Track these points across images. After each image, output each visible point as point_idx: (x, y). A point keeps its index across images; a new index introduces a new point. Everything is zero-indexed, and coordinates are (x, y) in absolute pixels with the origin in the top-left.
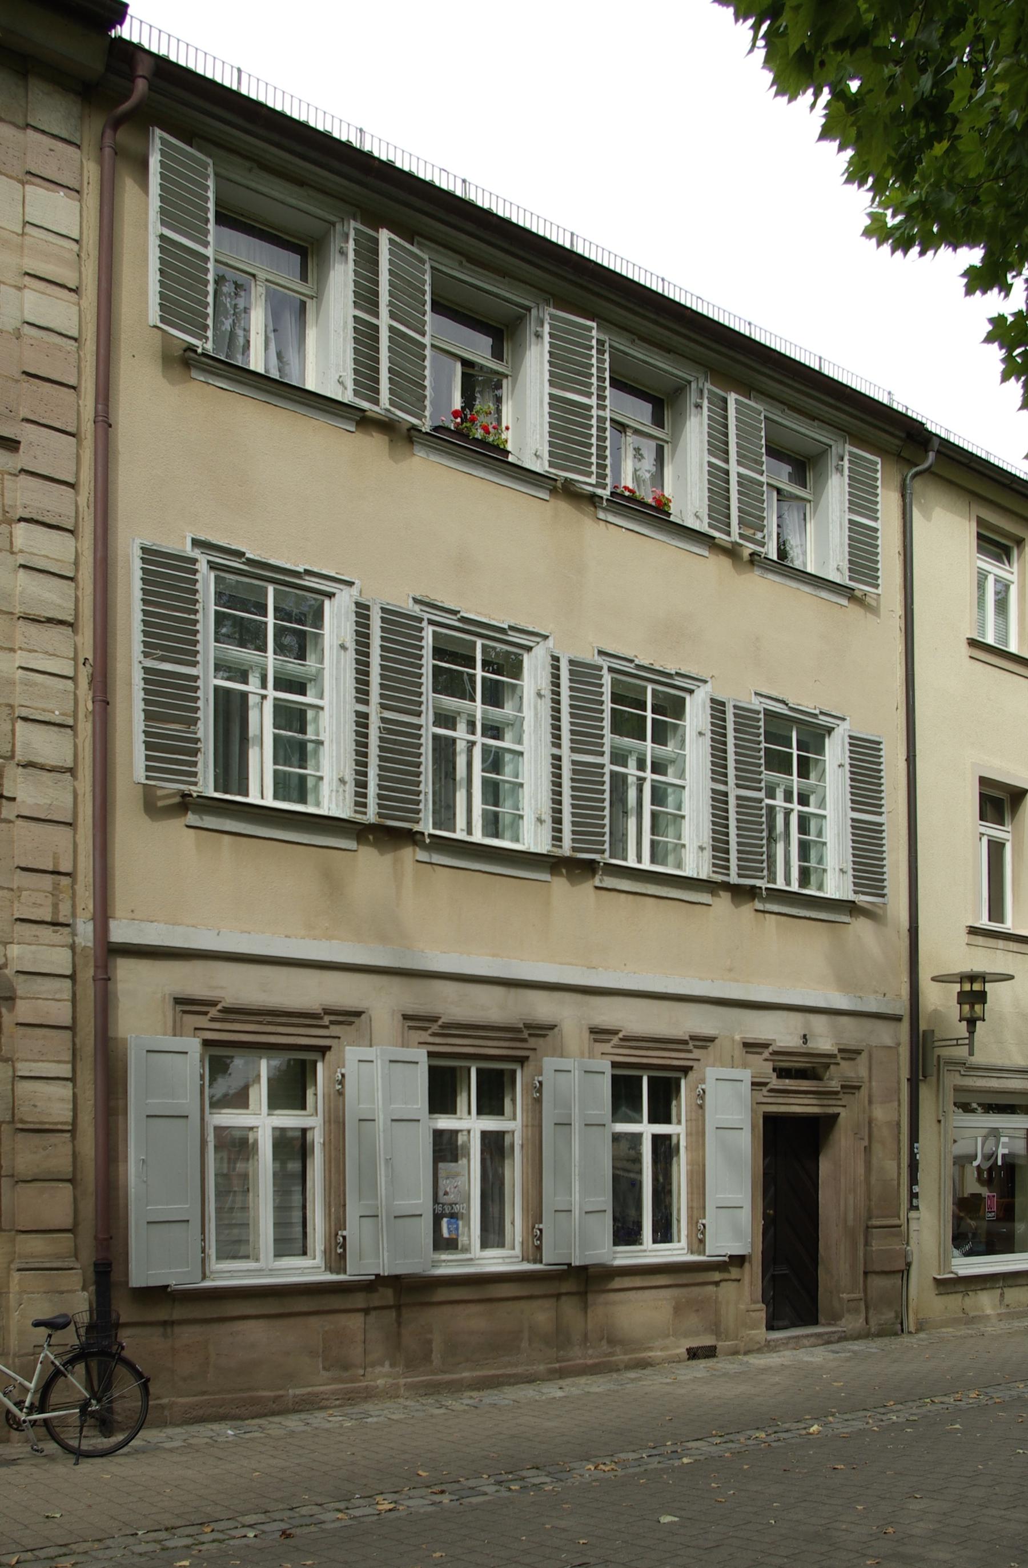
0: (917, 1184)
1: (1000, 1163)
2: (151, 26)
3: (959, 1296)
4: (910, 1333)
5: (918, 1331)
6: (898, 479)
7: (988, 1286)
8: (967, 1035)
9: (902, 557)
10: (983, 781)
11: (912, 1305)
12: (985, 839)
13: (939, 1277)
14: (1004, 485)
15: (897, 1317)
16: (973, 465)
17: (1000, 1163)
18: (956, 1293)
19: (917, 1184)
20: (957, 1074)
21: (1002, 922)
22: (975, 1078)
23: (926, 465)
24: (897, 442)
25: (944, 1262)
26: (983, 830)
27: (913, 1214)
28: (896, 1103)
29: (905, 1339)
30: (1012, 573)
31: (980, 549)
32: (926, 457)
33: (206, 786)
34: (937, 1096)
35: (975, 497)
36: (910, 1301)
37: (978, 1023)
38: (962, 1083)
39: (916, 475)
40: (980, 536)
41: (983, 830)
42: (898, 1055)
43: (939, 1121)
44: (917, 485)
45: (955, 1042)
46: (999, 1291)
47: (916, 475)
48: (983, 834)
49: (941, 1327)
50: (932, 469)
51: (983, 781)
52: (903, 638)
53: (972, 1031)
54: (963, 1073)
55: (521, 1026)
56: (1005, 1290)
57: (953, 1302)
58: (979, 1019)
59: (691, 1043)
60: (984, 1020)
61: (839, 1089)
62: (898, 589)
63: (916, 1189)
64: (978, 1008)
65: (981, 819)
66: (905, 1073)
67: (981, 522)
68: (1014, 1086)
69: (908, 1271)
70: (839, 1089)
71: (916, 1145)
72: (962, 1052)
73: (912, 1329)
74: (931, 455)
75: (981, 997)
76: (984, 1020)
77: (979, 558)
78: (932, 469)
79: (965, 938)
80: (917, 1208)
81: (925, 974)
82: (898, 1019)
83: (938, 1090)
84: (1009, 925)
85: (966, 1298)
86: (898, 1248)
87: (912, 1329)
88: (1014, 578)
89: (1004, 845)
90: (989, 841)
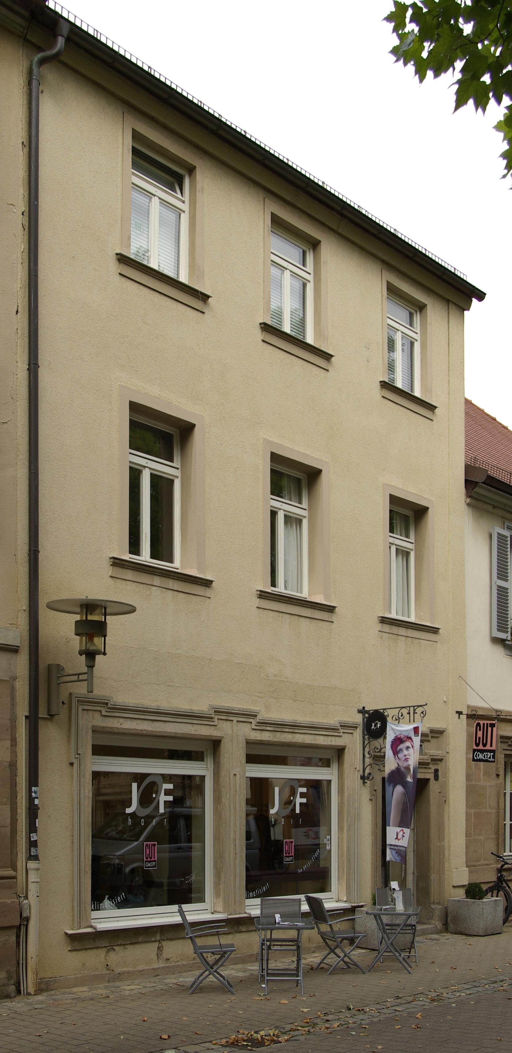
0: (35, 831)
1: (298, 811)
2: (75, 16)
3: (102, 952)
4: (29, 994)
5: (39, 991)
6: (26, 64)
7: (140, 939)
8: (85, 669)
9: (26, 150)
10: (134, 407)
11: (31, 964)
12: (393, 548)
13: (70, 932)
14: (408, 257)
15: (9, 977)
16: (267, 162)
17: (298, 811)
18: (97, 948)
19: (35, 831)
20: (97, 715)
21: (139, 555)
22: (121, 720)
23: (55, 51)
24: (18, 19)
25: (81, 918)
26: (391, 540)
27: (32, 865)
28: (8, 743)
29: (18, 1004)
30: (184, 202)
31: (135, 165)
32: (55, 42)
33: (145, 556)
34: (69, 737)
35: (129, 107)
36: (29, 958)
37: (98, 658)
38: (104, 725)
39: (42, 62)
40: (135, 151)
41: (391, 540)
42: (13, 689)
43: (72, 764)
44: (50, 75)
45: (75, 678)
46: (157, 944)
47: (42, 62)
48: (393, 544)
49: (75, 986)
50: (62, 58)
51: (134, 407)
52: (26, 237)
53: (91, 666)
54: (104, 713)
55: (212, 712)
56: (164, 943)
57: (95, 959)
58: (99, 653)
59: (341, 731)
60: (105, 654)
61: (430, 761)
62: (20, 183)
63: (34, 837)
64: (98, 641)
65: (391, 530)
66: (23, 710)
67: (136, 136)
68: (174, 731)
69: (27, 926)
70: (430, 761)
71: (34, 789)
72: (80, 689)
73: (31, 990)
74: (61, 41)
75: (100, 629)
76: (105, 654)
77: (133, 174)
78: (62, 58)
79: (109, 570)
80: (36, 858)
81: (43, 602)
82: (14, 650)
83: (69, 730)
84: (280, 589)
85: (112, 954)
86: (9, 901)
87: (31, 990)
88: (310, 278)
89: (172, 482)
90: (152, 475)
